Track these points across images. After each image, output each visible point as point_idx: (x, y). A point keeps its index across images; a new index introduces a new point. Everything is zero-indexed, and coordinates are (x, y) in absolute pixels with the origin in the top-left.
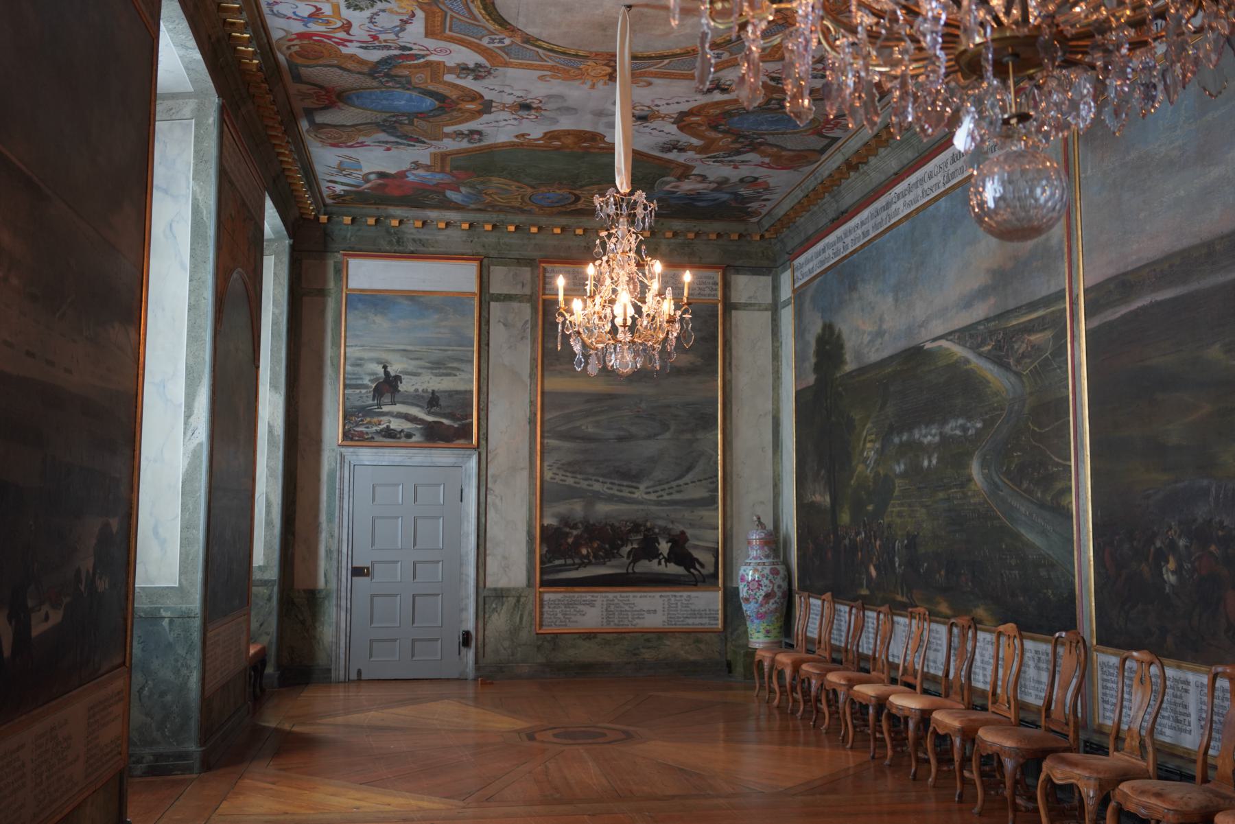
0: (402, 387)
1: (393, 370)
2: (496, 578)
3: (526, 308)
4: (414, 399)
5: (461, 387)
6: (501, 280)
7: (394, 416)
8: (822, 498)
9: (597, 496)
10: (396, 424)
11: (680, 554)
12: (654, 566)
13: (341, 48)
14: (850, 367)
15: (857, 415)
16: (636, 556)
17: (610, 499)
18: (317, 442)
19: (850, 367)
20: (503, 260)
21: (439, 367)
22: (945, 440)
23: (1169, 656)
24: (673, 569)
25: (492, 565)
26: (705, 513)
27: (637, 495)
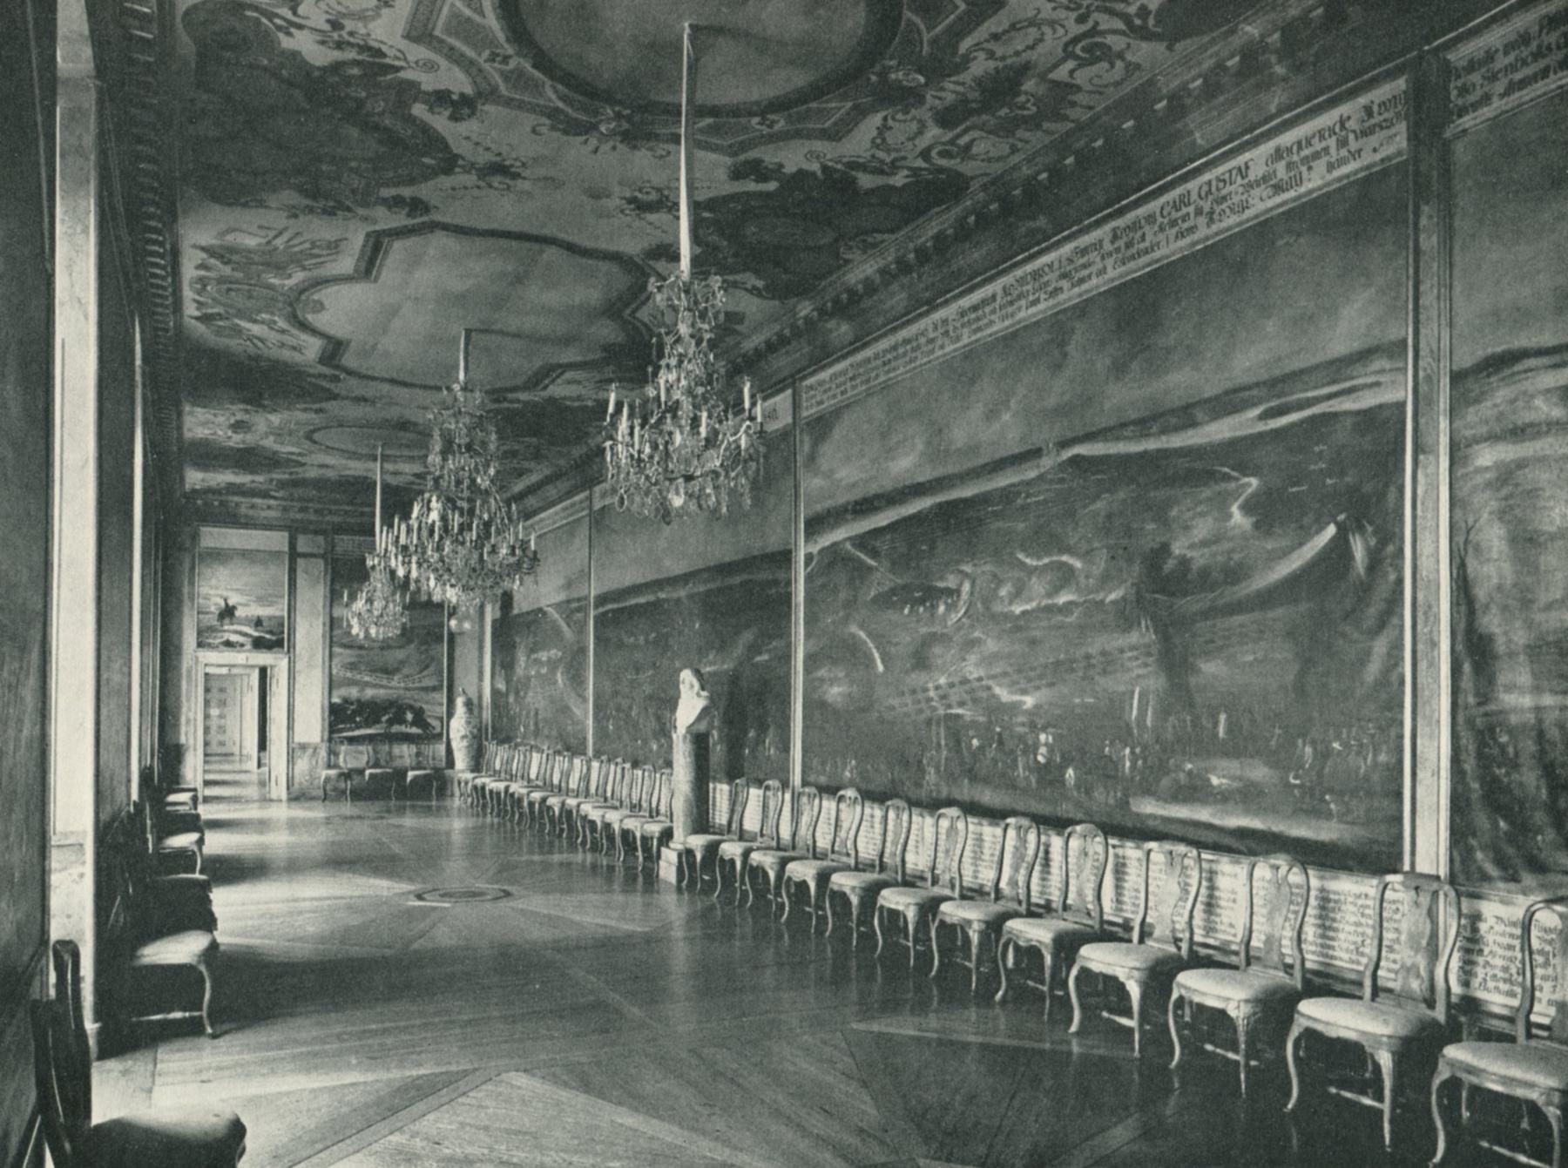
0: (237, 613)
1: (231, 603)
2: (299, 738)
3: (321, 563)
4: (247, 621)
5: (278, 613)
6: (303, 544)
7: (231, 632)
8: (502, 686)
9: (367, 684)
10: (234, 638)
11: (419, 719)
12: (403, 729)
13: (281, 36)
14: (516, 611)
15: (518, 640)
16: (391, 722)
17: (375, 686)
18: (178, 650)
19: (516, 611)
20: (305, 531)
21: (261, 600)
22: (549, 659)
23: (1313, 863)
24: (415, 730)
25: (1418, 859)
26: (436, 695)
27: (394, 683)
